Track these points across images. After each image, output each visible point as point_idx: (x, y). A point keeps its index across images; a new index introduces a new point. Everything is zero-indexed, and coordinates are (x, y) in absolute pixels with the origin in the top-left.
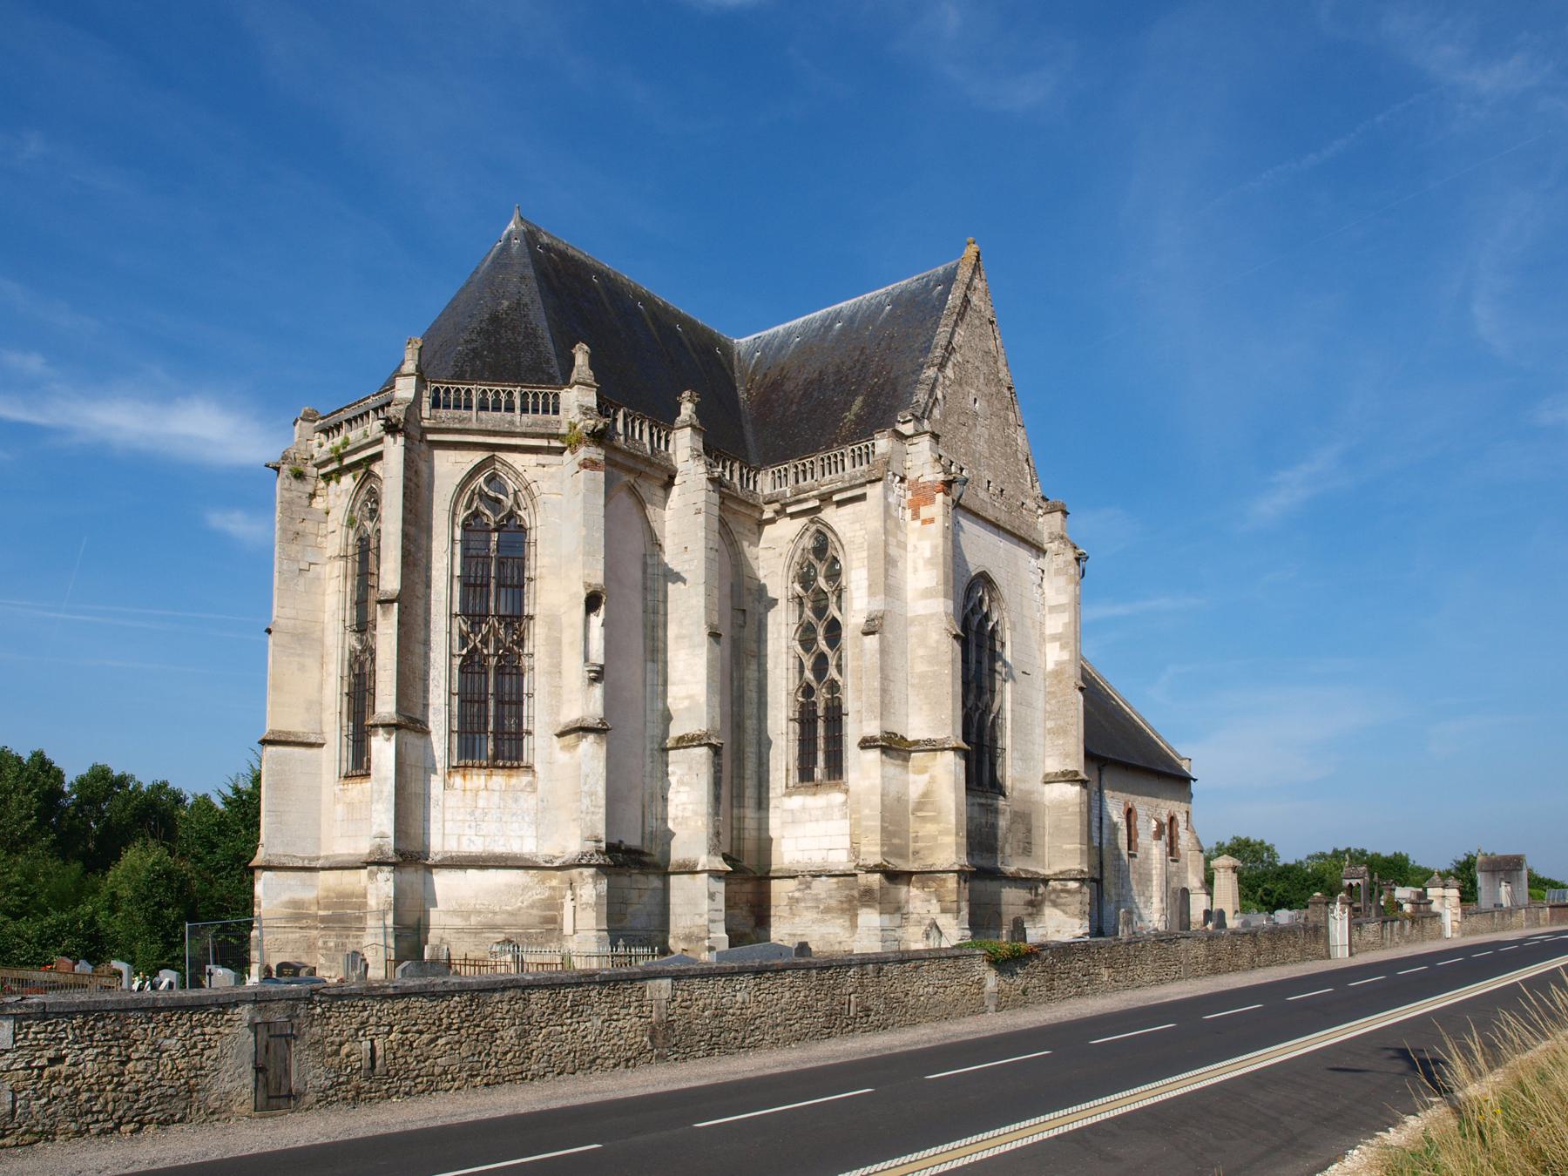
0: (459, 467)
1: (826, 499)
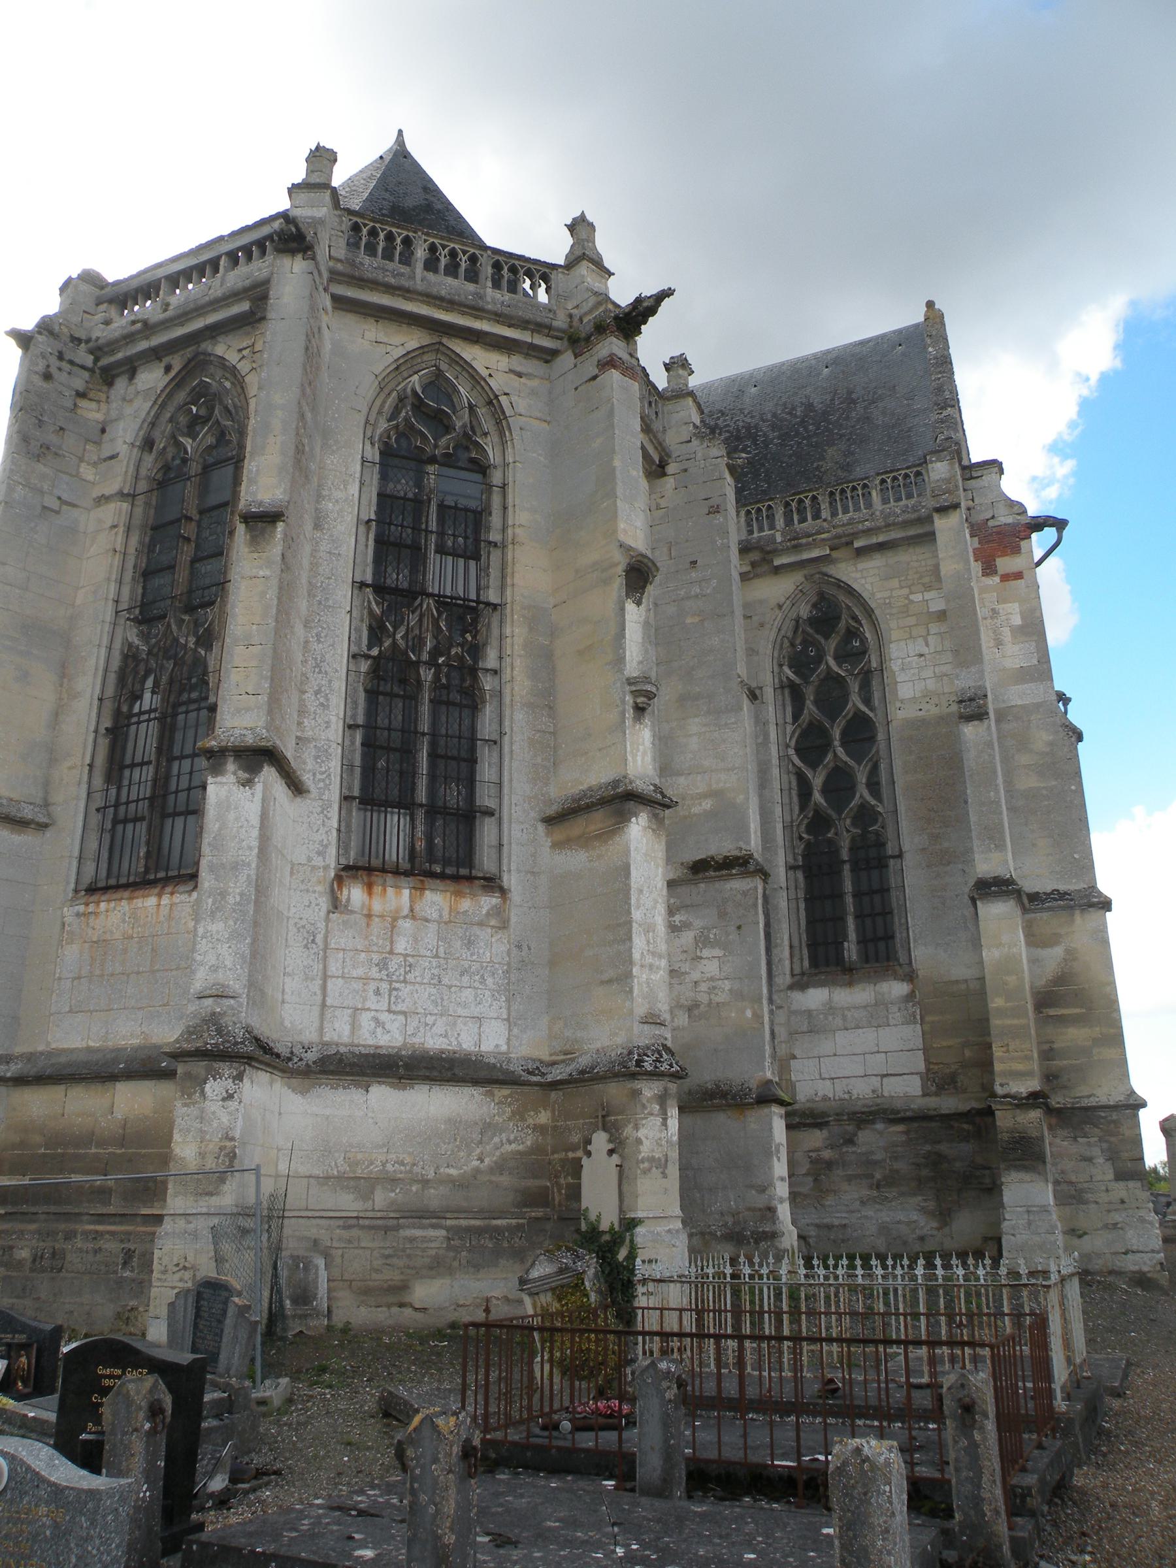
0: (382, 349)
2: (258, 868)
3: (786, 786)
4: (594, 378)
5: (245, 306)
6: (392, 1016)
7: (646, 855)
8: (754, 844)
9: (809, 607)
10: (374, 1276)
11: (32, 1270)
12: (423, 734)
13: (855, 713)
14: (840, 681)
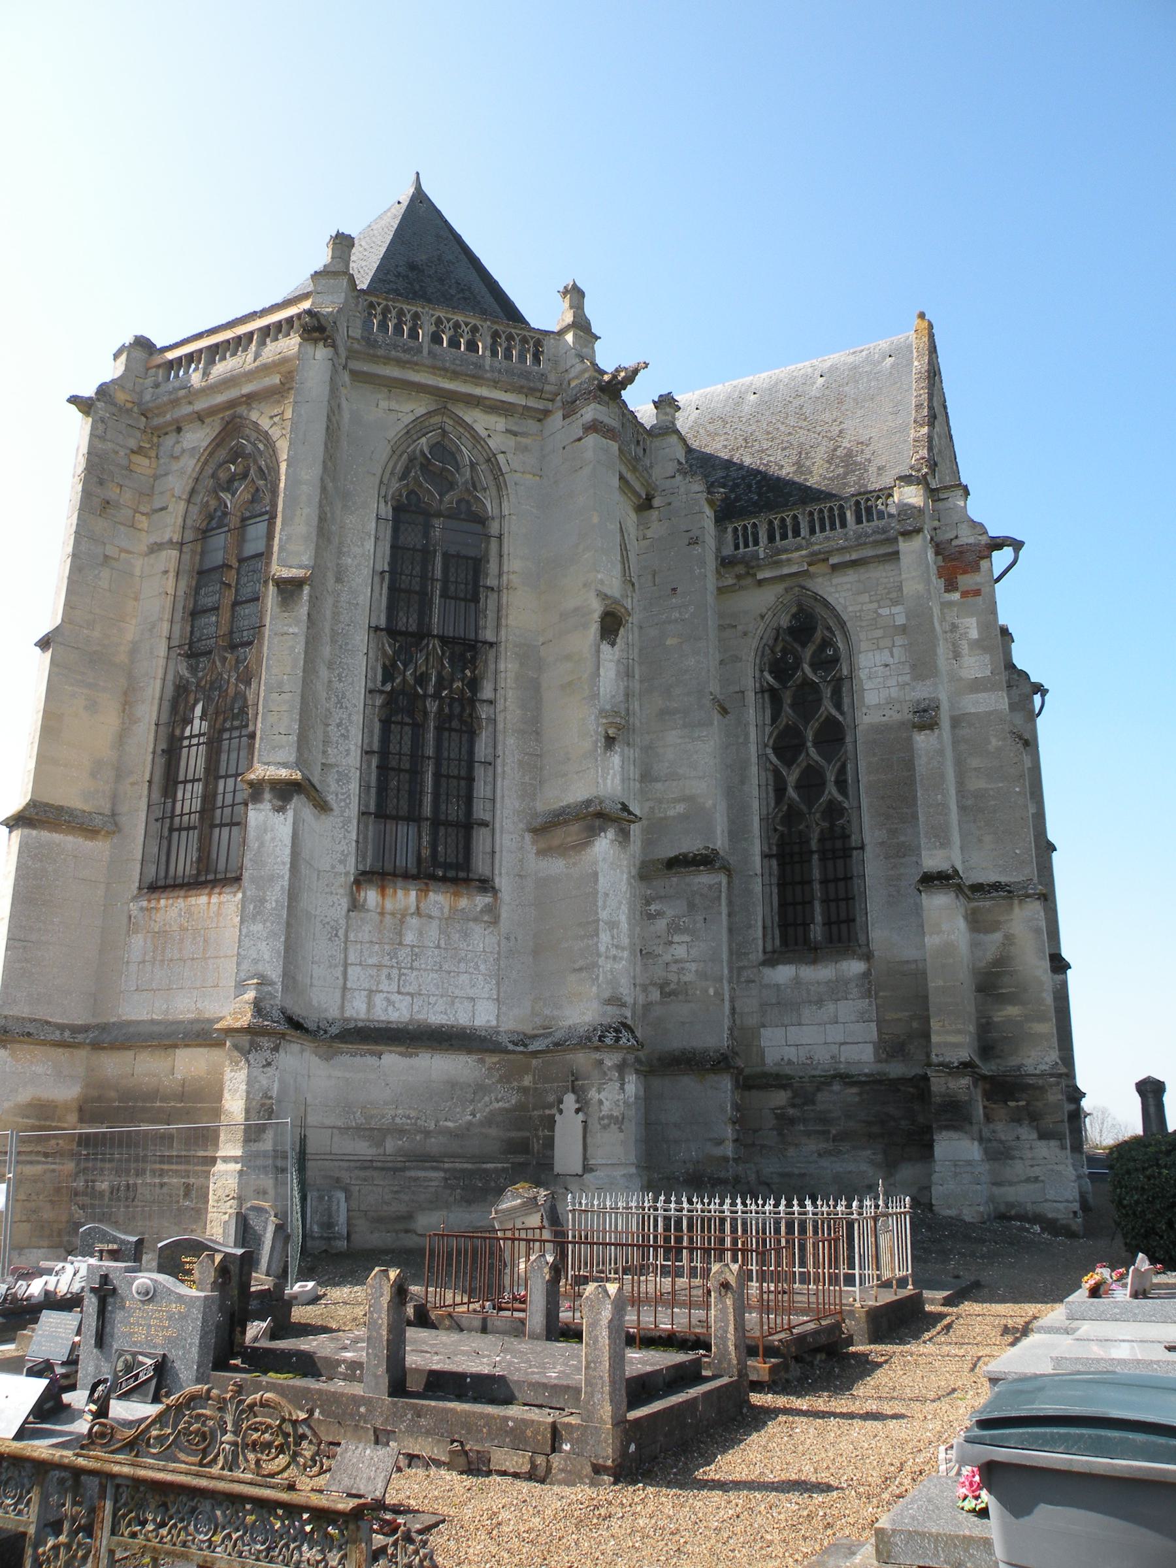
1: (818, 558)
2: (290, 879)
3: (763, 782)
4: (580, 439)
5: (276, 379)
6: (400, 997)
7: (612, 864)
8: (720, 842)
9: (789, 617)
10: (385, 1208)
11: (111, 1200)
12: (429, 758)
13: (827, 717)
14: (814, 687)
